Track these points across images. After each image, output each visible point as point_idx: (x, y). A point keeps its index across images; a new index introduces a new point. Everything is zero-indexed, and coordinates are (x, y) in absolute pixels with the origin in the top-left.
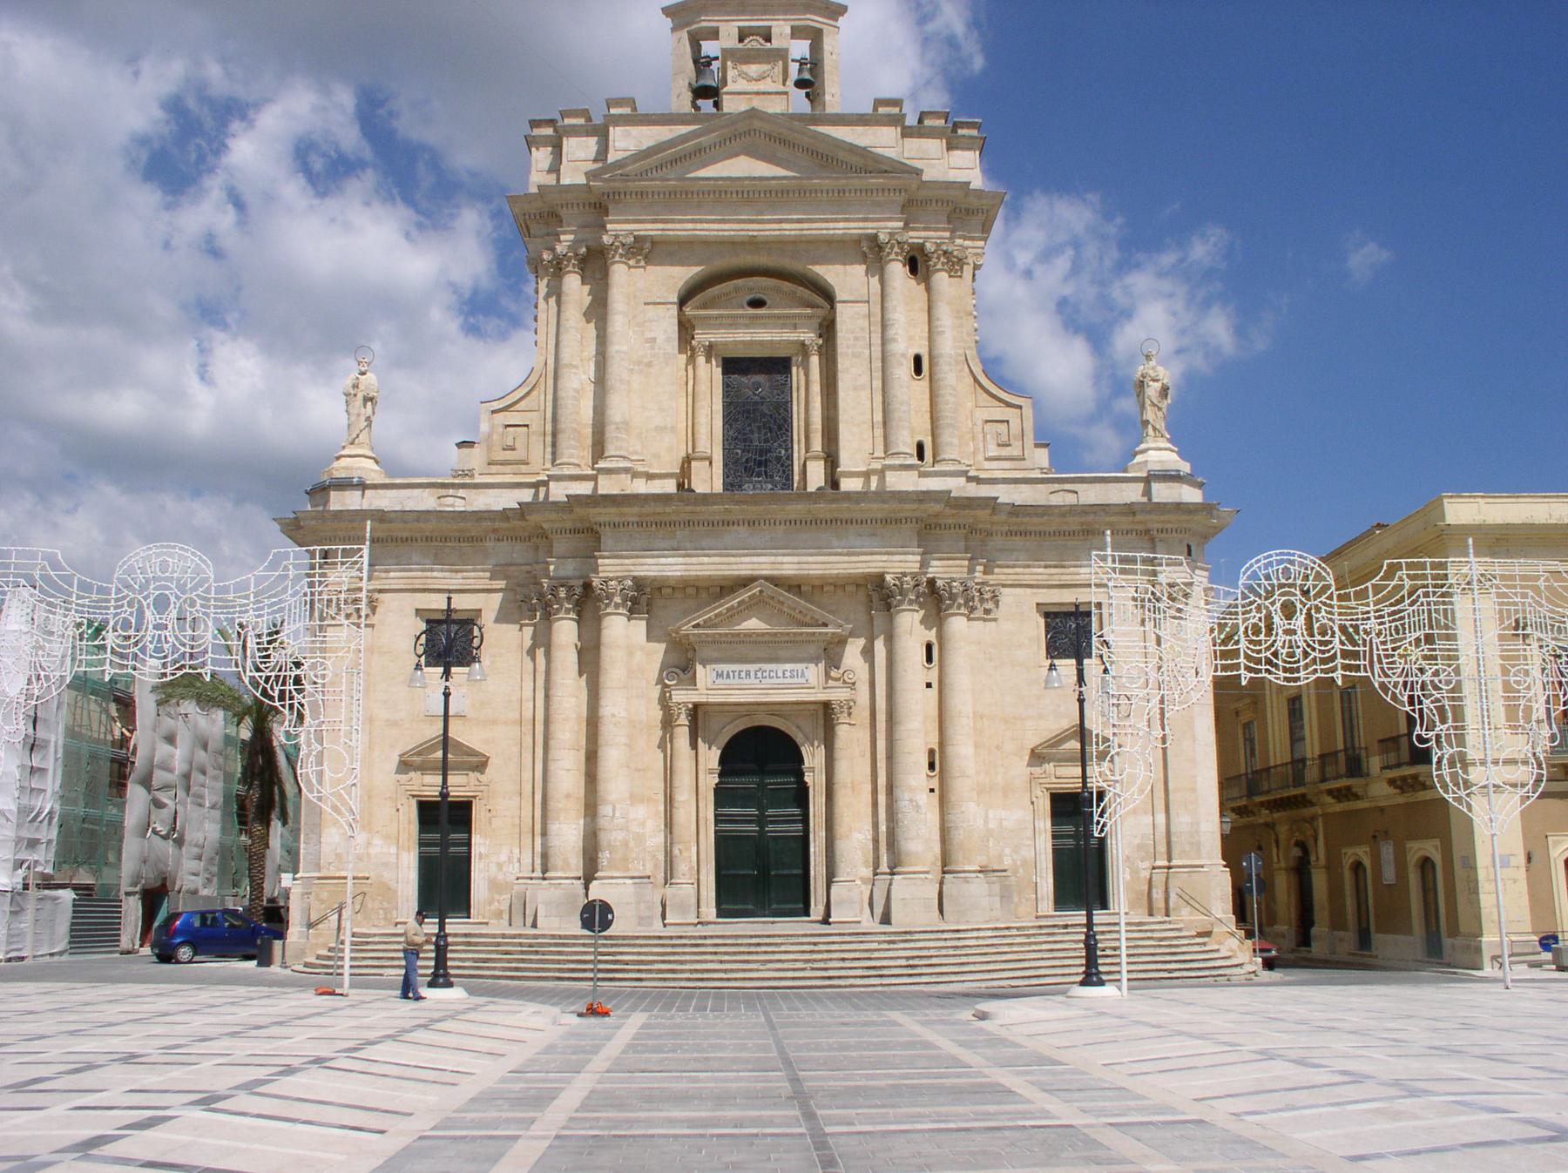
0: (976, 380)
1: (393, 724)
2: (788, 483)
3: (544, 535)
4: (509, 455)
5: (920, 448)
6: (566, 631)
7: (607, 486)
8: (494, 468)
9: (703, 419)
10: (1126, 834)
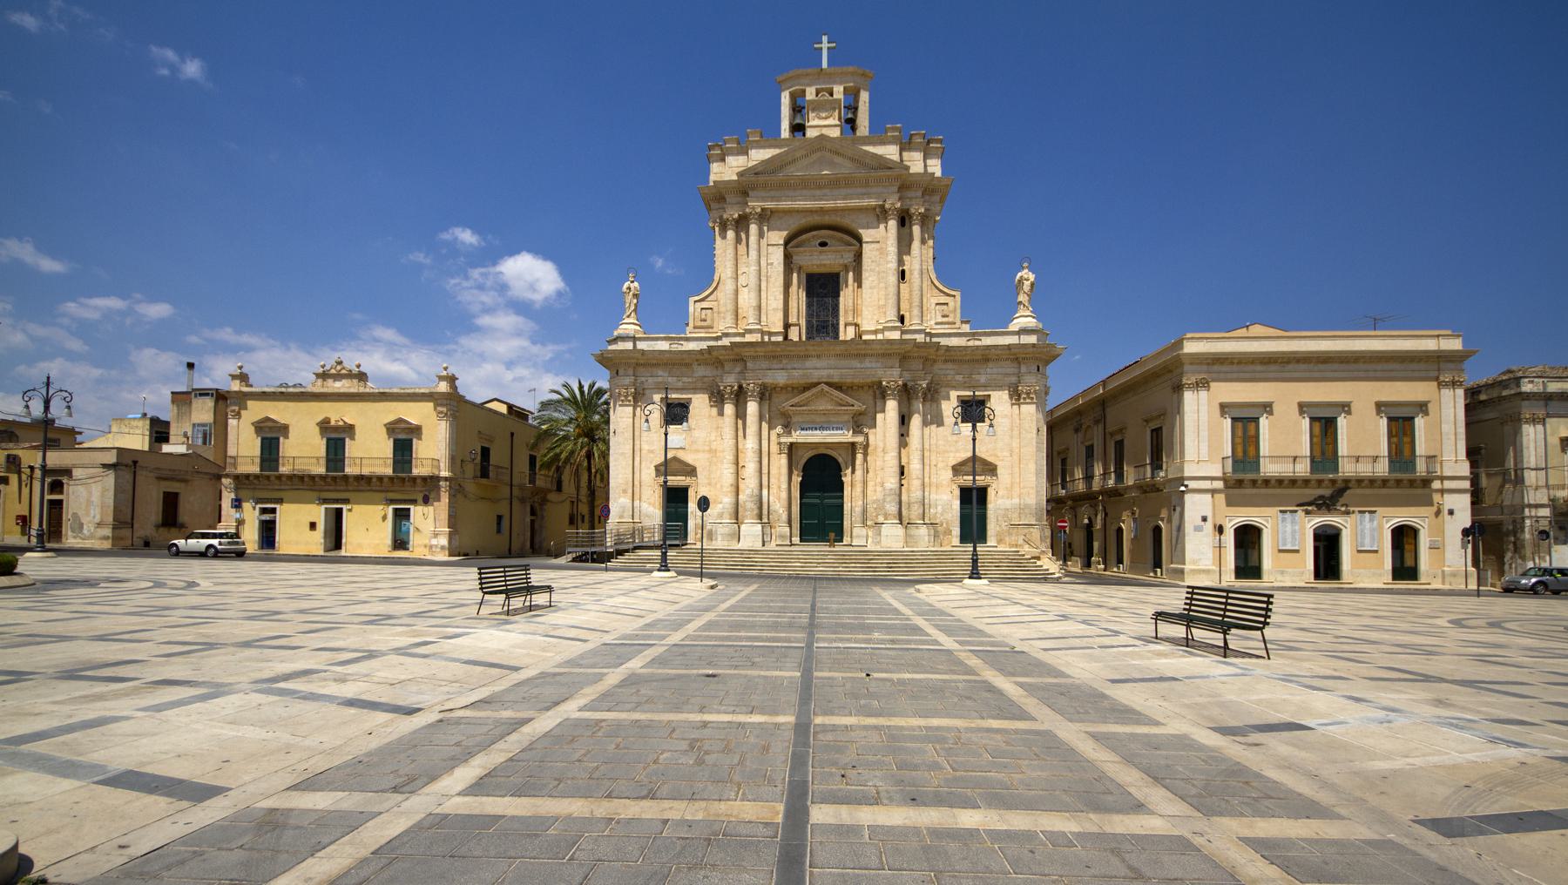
1: (651, 452)
6: (729, 409)
10: (997, 503)
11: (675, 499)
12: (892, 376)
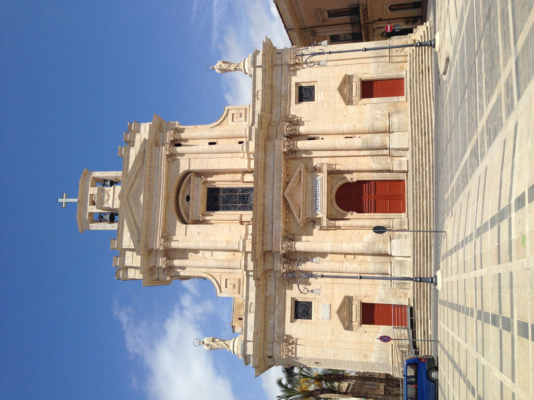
0: (218, 125)
2: (251, 189)
3: (265, 272)
4: (237, 286)
5: (241, 143)
7: (249, 248)
8: (241, 292)
9: (227, 217)
11: (370, 314)
12: (281, 146)
